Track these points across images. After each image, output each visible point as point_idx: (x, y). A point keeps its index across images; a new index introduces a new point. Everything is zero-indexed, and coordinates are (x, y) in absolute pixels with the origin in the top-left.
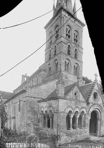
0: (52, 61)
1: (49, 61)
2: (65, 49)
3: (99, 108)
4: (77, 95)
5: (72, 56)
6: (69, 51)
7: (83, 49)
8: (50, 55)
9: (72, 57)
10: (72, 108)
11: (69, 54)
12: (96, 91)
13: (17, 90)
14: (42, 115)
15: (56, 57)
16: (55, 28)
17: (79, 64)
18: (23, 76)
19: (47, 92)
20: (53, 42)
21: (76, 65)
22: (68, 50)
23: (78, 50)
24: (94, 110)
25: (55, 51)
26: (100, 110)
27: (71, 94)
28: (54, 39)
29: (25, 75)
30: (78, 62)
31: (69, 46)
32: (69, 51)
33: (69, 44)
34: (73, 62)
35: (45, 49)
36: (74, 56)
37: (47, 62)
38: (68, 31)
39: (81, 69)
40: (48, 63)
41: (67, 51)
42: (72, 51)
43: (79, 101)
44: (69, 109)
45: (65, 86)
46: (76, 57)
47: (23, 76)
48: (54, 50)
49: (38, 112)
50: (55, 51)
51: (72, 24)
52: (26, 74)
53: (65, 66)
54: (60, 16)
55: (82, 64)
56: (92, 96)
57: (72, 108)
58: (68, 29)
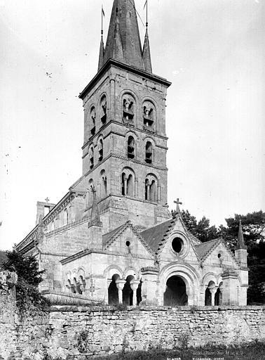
0: (97, 171)
1: (90, 172)
2: (121, 146)
3: (187, 271)
4: (131, 245)
5: (138, 159)
6: (130, 150)
7: (167, 139)
8: (92, 160)
9: (138, 162)
10: (120, 270)
11: (131, 156)
12: (178, 236)
13: (23, 242)
14: (69, 288)
15: (102, 166)
16: (101, 103)
17: (157, 174)
18: (39, 204)
19: (79, 242)
20: (97, 130)
21: (151, 178)
22: (129, 148)
23: (153, 144)
24: (172, 275)
25: (101, 152)
26: (189, 273)
27: (119, 245)
28: (99, 125)
29: (45, 201)
30: (155, 172)
31: (131, 138)
32: (130, 150)
33: (131, 134)
34: (141, 171)
35: (82, 145)
36: (143, 158)
37: (86, 175)
38: (127, 106)
39: (163, 186)
40: (88, 178)
41: (125, 152)
42: (140, 150)
43: (136, 257)
44: (113, 272)
45: (103, 232)
46: (149, 161)
47: (39, 204)
48: (100, 149)
49: (62, 283)
50: (101, 152)
51: (135, 89)
52: (47, 200)
53: (123, 182)
54: (108, 77)
55: (166, 175)
56: (168, 245)
57: (120, 270)
58: (127, 101)
